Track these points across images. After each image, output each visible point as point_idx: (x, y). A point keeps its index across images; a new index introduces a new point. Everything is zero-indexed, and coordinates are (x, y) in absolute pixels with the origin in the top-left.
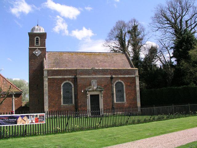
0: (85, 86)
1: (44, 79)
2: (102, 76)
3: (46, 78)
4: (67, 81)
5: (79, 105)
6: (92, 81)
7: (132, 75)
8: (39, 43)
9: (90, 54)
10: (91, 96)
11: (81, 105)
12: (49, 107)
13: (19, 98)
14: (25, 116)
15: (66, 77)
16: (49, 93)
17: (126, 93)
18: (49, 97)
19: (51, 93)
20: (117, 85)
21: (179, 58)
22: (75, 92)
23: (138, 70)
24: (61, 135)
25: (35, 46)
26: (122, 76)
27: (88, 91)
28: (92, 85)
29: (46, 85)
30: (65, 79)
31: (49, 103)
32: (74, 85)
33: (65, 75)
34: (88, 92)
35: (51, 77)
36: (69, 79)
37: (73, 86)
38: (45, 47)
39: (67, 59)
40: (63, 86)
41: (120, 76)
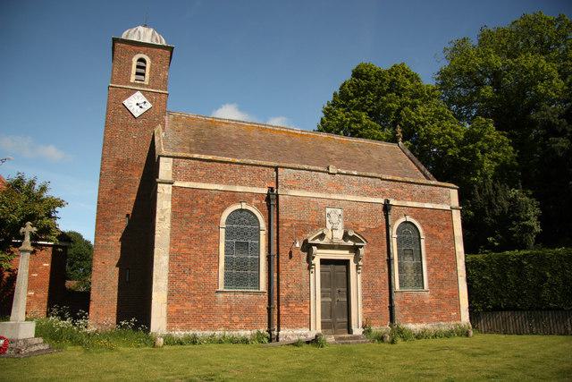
0: (303, 227)
1: (159, 190)
7: (443, 202)
8: (147, 74)
10: (323, 262)
11: (289, 297)
13: (497, 132)
15: (239, 189)
16: (172, 244)
17: (428, 260)
18: (173, 258)
21: (479, 174)
25: (132, 84)
26: (415, 204)
27: (315, 245)
28: (329, 226)
30: (234, 197)
34: (314, 248)
35: (186, 184)
37: (263, 225)
39: (234, 137)
40: (229, 220)
41: (410, 204)
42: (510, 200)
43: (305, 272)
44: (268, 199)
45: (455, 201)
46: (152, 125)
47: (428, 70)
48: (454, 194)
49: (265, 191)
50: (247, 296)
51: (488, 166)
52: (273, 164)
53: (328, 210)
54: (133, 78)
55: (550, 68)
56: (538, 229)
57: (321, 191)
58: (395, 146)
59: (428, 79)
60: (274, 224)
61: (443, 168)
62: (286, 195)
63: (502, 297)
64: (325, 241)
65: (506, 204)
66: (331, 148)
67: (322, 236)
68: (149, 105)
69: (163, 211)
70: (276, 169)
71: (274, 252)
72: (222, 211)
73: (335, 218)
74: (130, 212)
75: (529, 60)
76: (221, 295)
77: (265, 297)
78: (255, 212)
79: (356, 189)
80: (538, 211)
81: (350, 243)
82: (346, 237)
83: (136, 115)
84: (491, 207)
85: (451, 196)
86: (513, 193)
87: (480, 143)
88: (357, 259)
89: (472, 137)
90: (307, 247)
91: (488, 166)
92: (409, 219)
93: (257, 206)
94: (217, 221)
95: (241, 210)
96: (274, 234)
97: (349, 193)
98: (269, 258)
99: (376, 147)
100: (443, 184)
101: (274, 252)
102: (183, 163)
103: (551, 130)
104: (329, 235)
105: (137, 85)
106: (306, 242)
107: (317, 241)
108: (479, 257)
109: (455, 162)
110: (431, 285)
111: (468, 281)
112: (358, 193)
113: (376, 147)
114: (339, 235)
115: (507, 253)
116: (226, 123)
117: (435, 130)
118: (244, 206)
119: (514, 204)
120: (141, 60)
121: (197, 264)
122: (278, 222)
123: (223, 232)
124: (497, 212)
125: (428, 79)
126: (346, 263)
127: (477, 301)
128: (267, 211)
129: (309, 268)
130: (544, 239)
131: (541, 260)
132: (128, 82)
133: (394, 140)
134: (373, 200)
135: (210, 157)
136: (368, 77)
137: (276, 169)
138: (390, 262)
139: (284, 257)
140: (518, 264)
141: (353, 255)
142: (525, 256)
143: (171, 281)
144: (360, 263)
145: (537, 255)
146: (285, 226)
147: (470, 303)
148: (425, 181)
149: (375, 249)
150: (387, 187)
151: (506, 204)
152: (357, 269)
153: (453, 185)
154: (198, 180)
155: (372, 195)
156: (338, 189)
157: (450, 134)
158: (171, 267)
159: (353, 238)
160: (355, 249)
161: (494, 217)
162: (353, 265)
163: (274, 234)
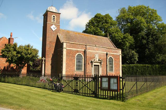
0: (91, 58)
8: (55, 20)
10: (95, 65)
15: (79, 50)
18: (66, 64)
26: (112, 54)
28: (96, 58)
30: (78, 52)
37: (83, 57)
41: (111, 53)
42: (132, 53)
43: (91, 67)
44: (84, 52)
45: (120, 53)
46: (57, 33)
47: (114, 14)
48: (120, 51)
49: (84, 50)
50: (80, 72)
51: (128, 44)
52: (85, 44)
53: (96, 55)
54: (52, 21)
55: (143, 20)
56: (137, 60)
57: (94, 51)
58: (107, 38)
59: (114, 19)
60: (85, 57)
61: (118, 44)
62: (88, 51)
63: (129, 74)
64: (95, 61)
65: (131, 54)
66: (94, 39)
67: (94, 60)
68: (56, 28)
69: (64, 54)
70: (86, 45)
71: (85, 63)
72: (76, 54)
73: (97, 56)
74: (53, 53)
75: (139, 18)
76: (75, 72)
77: (83, 72)
78: (82, 55)
79: (101, 50)
80: (138, 56)
81: (100, 62)
82: (99, 60)
83: (54, 30)
84: (128, 55)
85: (120, 52)
86: (133, 52)
87: (126, 39)
88: (101, 65)
89: (125, 38)
90: (92, 62)
91: (128, 44)
92: (111, 57)
93: (82, 53)
94: (75, 57)
95: (79, 54)
96: (85, 60)
97: (100, 51)
98: (84, 64)
99: (103, 38)
100: (118, 49)
101: (85, 63)
102: (68, 44)
103: (143, 38)
104: (96, 60)
105: (53, 23)
106: (91, 61)
107: (94, 61)
108: (125, 65)
109: (120, 43)
110: (115, 71)
111: (122, 70)
112: (101, 51)
113: (103, 38)
114: (98, 60)
115: (131, 65)
116: (71, 32)
117: (116, 35)
118: (80, 53)
119: (133, 53)
120: (54, 16)
121: (71, 65)
122: (86, 57)
123: (76, 59)
124: (129, 56)
125: (114, 19)
126: (98, 66)
127: (124, 75)
128: (84, 55)
129: (92, 67)
130: (138, 62)
131: (137, 67)
132: (51, 22)
133: (106, 36)
134: (103, 52)
135: (73, 43)
136: (99, 18)
137: (86, 45)
138: (107, 66)
139: (87, 64)
140: (133, 67)
141: (100, 64)
142: (134, 66)
143: (66, 69)
144: (102, 66)
145: (137, 66)
146: (87, 58)
147: (122, 75)
148: (114, 48)
149: (104, 63)
150: (107, 50)
151: (131, 54)
152: (101, 67)
153: (120, 49)
154: (71, 48)
155: (104, 51)
156: (98, 50)
157: (120, 36)
158: (66, 66)
159: (100, 61)
160: (101, 63)
161: (128, 57)
162: (100, 66)
163: (85, 60)
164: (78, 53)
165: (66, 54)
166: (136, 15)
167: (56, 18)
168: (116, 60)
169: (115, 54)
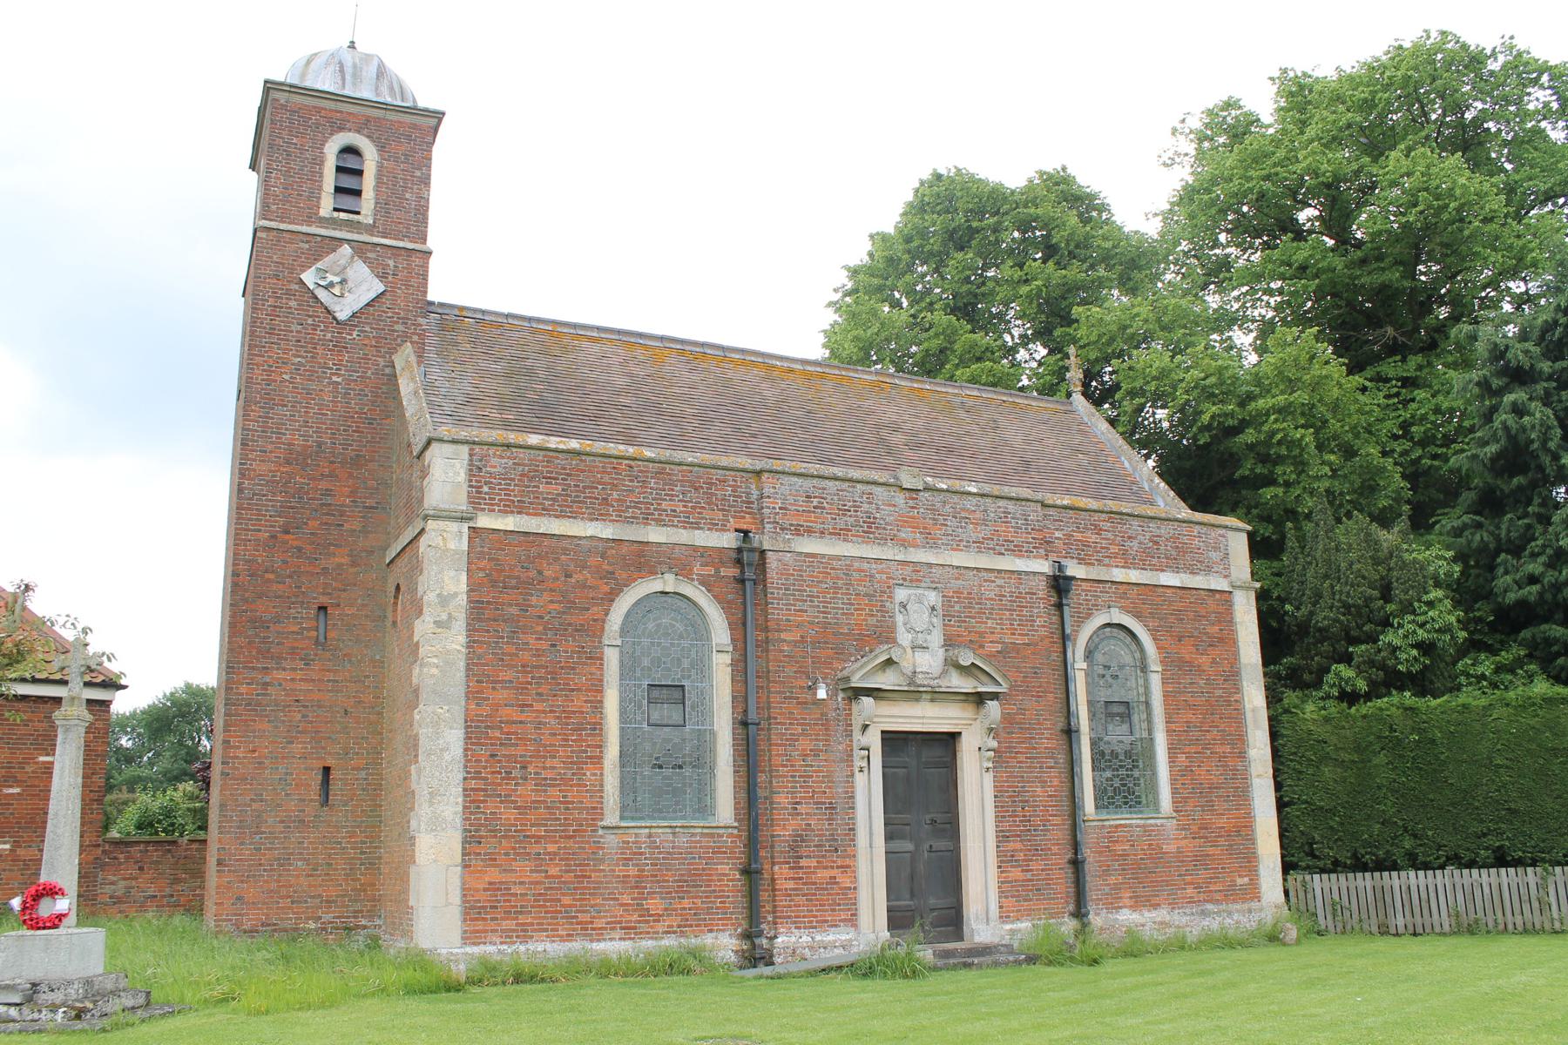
2: (985, 561)
3: (453, 527)
4: (669, 582)
5: (784, 831)
6: (901, 594)
9: (743, 363)
10: (893, 740)
11: (798, 840)
12: (471, 840)
14: (348, 241)
15: (655, 535)
16: (473, 695)
18: (475, 733)
19: (502, 694)
20: (1099, 657)
22: (740, 700)
23: (1244, 536)
24: (528, 986)
26: (1134, 576)
28: (904, 638)
29: (444, 600)
30: (643, 560)
31: (473, 800)
32: (739, 628)
33: (646, 519)
35: (509, 523)
36: (680, 561)
38: (424, 240)
41: (1119, 574)
53: (901, 594)
57: (883, 541)
72: (611, 597)
112: (980, 546)
132: (312, 217)
153: (1241, 525)
154: (544, 511)
155: (1018, 551)
164: (655, 585)
165: (462, 600)
166: (1377, 143)
167: (380, 168)
168: (1187, 652)
169: (1169, 579)
